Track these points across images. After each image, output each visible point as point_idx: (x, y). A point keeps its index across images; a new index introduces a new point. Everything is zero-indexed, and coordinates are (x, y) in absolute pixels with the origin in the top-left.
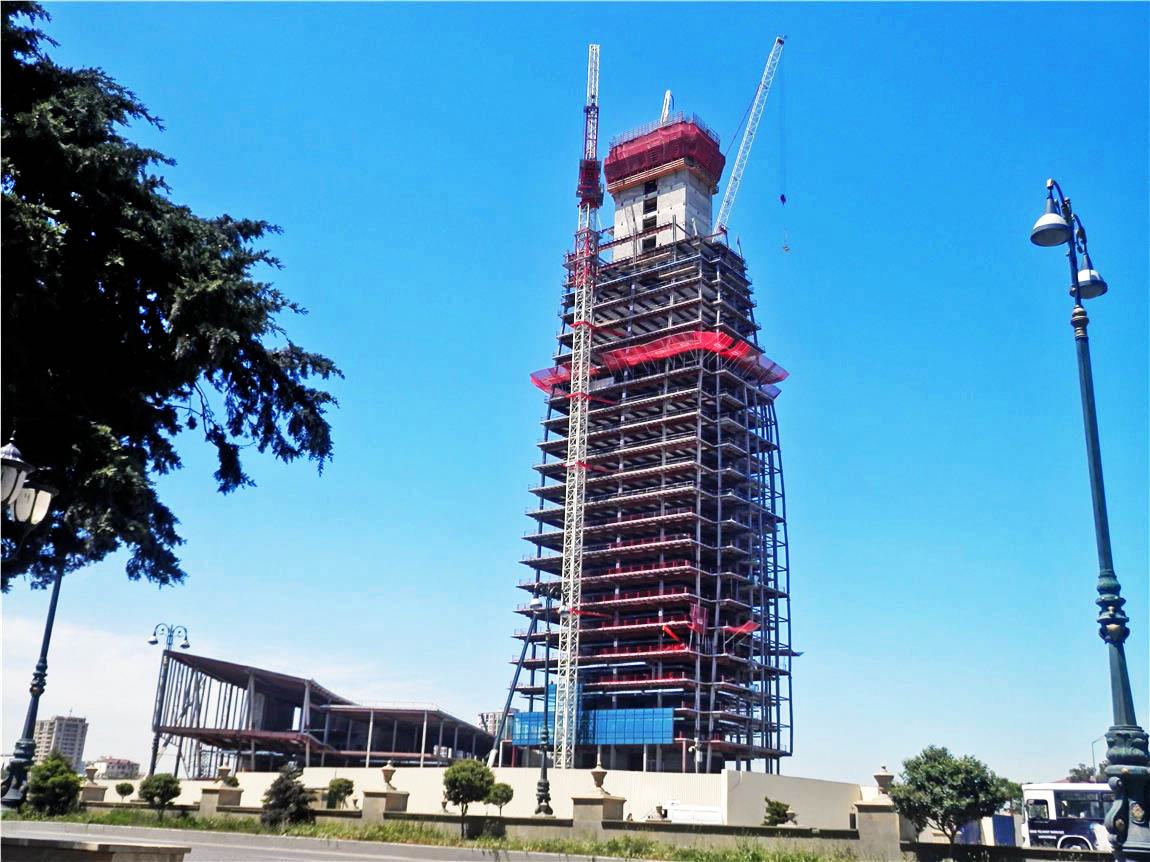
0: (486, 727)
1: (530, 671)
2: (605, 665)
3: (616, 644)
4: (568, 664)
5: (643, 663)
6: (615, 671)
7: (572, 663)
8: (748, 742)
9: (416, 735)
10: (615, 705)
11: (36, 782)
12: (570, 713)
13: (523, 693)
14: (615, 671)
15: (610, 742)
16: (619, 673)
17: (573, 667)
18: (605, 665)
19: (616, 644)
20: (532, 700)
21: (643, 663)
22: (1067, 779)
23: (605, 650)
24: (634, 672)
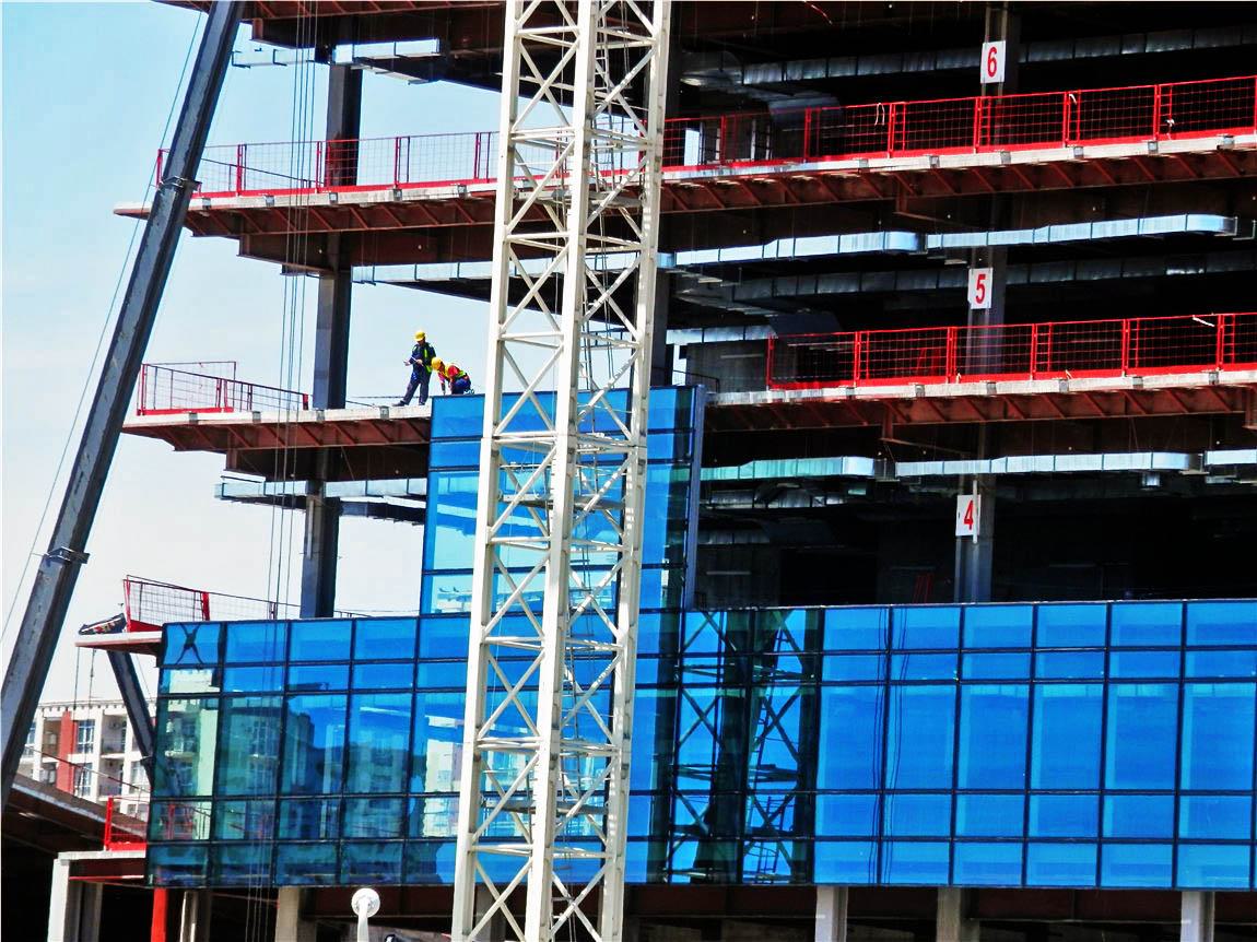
0: (794, 698)
1: (310, 286)
2: (901, 241)
3: (993, 61)
4: (573, 227)
5: (1212, 223)
6: (980, 291)
7: (613, 226)
8: (208, 800)
9: (134, 886)
10: (977, 562)
11: (1067, 143)
12: (582, 626)
13: (241, 464)
14: (980, 291)
15: (913, 866)
16: (1013, 303)
17: (620, 261)
18: (901, 241)
19: (993, 61)
20: (327, 518)
21: (1212, 223)
22: (526, 883)
23: (887, 112)
24: (848, 312)
